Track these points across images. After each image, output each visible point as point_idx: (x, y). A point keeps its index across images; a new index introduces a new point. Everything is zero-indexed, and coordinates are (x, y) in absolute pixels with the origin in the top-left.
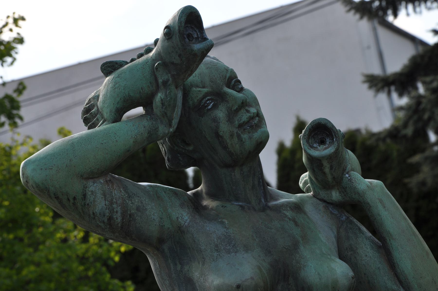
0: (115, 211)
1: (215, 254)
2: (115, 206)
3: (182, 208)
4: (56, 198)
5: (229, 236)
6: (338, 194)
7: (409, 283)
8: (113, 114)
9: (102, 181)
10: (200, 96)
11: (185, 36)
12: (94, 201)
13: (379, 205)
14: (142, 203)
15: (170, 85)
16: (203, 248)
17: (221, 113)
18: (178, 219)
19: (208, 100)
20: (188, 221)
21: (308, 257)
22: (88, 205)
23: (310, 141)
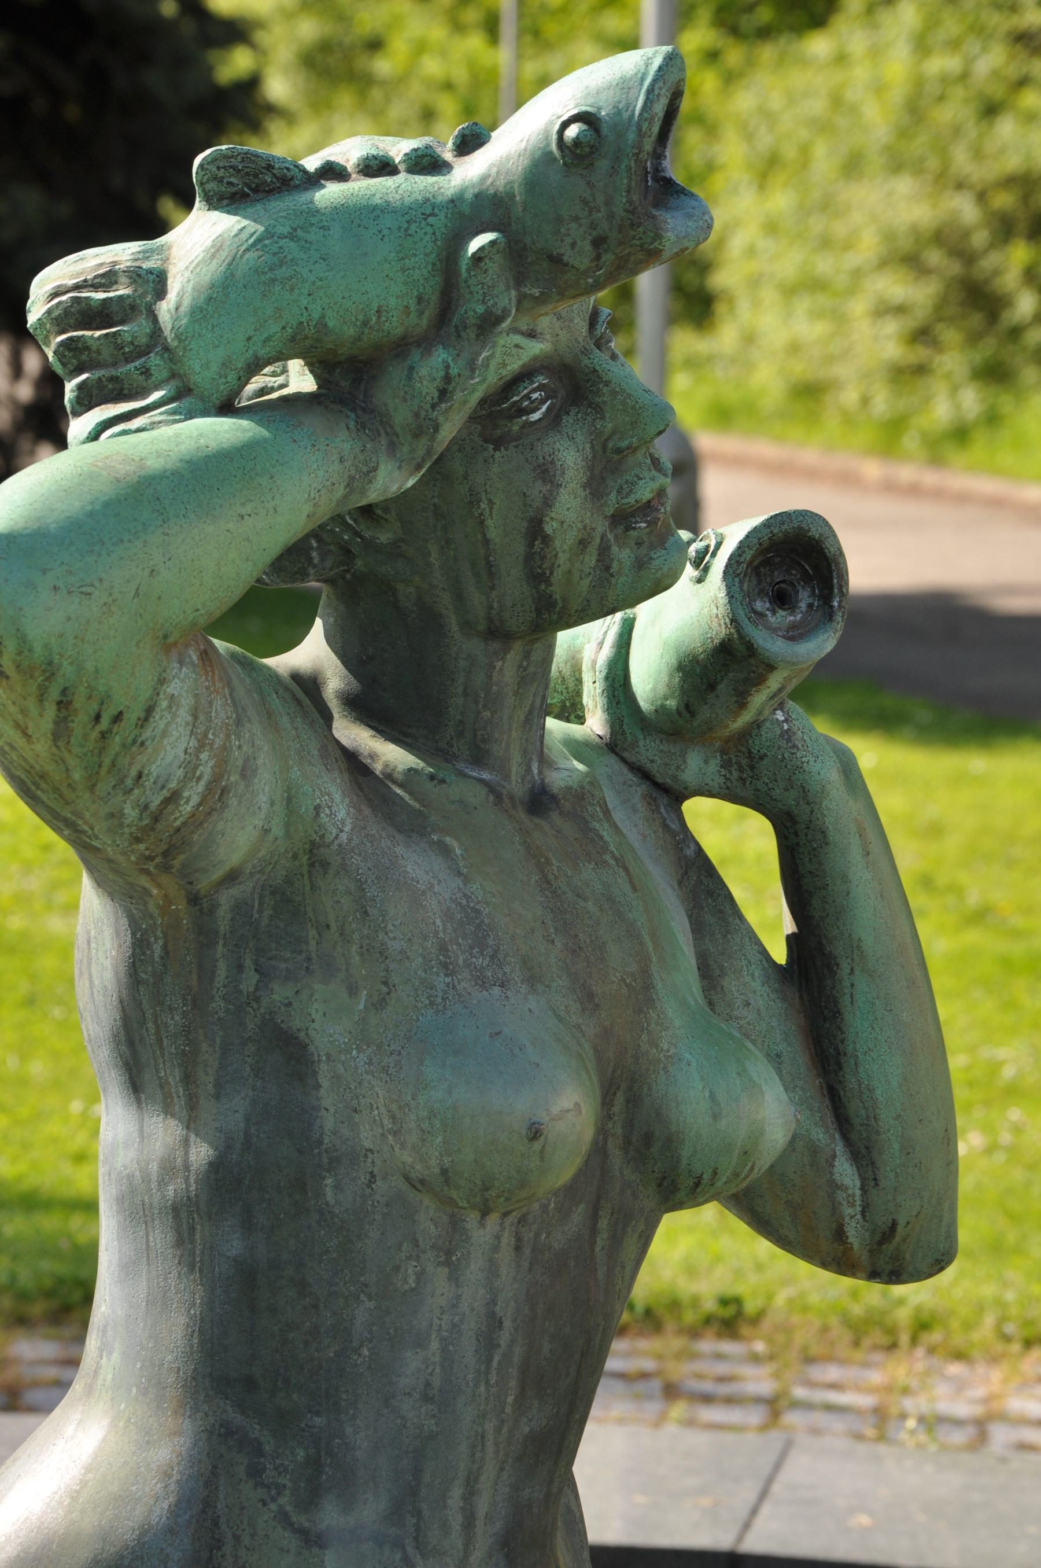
0: (198, 773)
1: (441, 981)
5: (478, 912)
7: (878, 1133)
10: (515, 366)
16: (394, 946)
18: (317, 815)
22: (142, 744)
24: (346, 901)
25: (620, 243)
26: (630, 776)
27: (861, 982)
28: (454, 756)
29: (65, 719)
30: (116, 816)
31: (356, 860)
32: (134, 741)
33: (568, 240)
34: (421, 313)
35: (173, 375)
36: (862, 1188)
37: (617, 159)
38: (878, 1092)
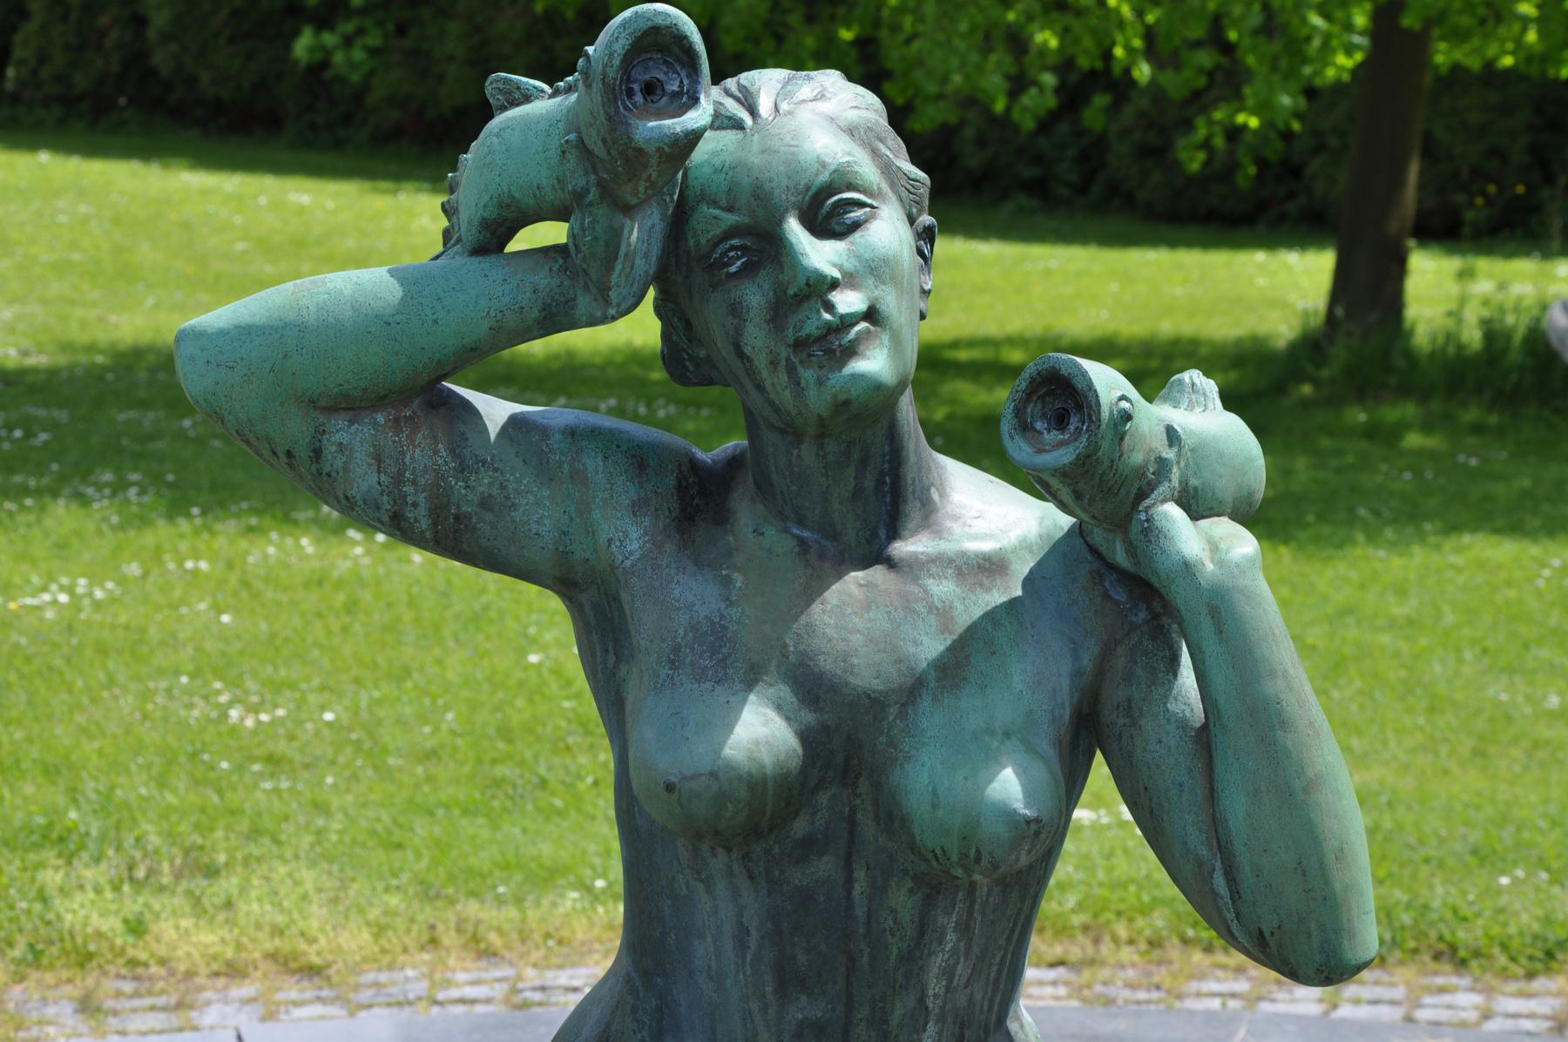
1: (665, 671)
2: (408, 489)
3: (634, 514)
5: (724, 628)
10: (716, 231)
11: (636, 87)
12: (346, 470)
14: (503, 487)
15: (591, 204)
17: (754, 296)
19: (732, 248)
20: (637, 555)
22: (329, 475)
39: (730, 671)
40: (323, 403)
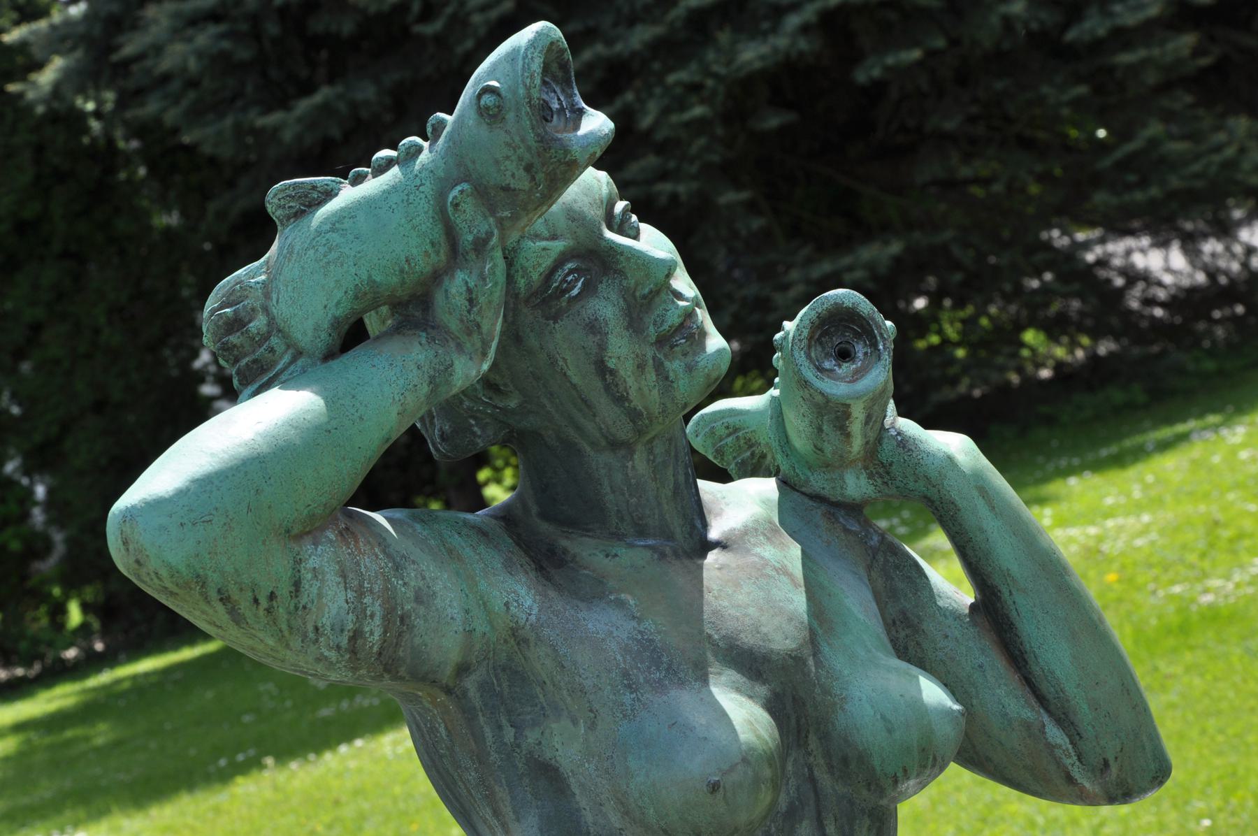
0: (368, 613)
1: (628, 698)
4: (221, 600)
5: (651, 641)
6: (863, 480)
7: (1068, 701)
8: (324, 336)
9: (332, 536)
10: (547, 262)
12: (320, 596)
13: (980, 503)
14: (424, 578)
16: (588, 683)
19: (571, 272)
21: (846, 672)
22: (304, 607)
23: (813, 355)
24: (548, 662)
25: (543, 165)
26: (811, 503)
27: (1019, 598)
28: (624, 535)
29: (233, 608)
30: (320, 659)
31: (546, 631)
32: (296, 608)
33: (509, 173)
34: (438, 253)
35: (288, 347)
36: (1071, 743)
37: (518, 110)
38: (1058, 672)
39: (682, 675)
40: (295, 531)
